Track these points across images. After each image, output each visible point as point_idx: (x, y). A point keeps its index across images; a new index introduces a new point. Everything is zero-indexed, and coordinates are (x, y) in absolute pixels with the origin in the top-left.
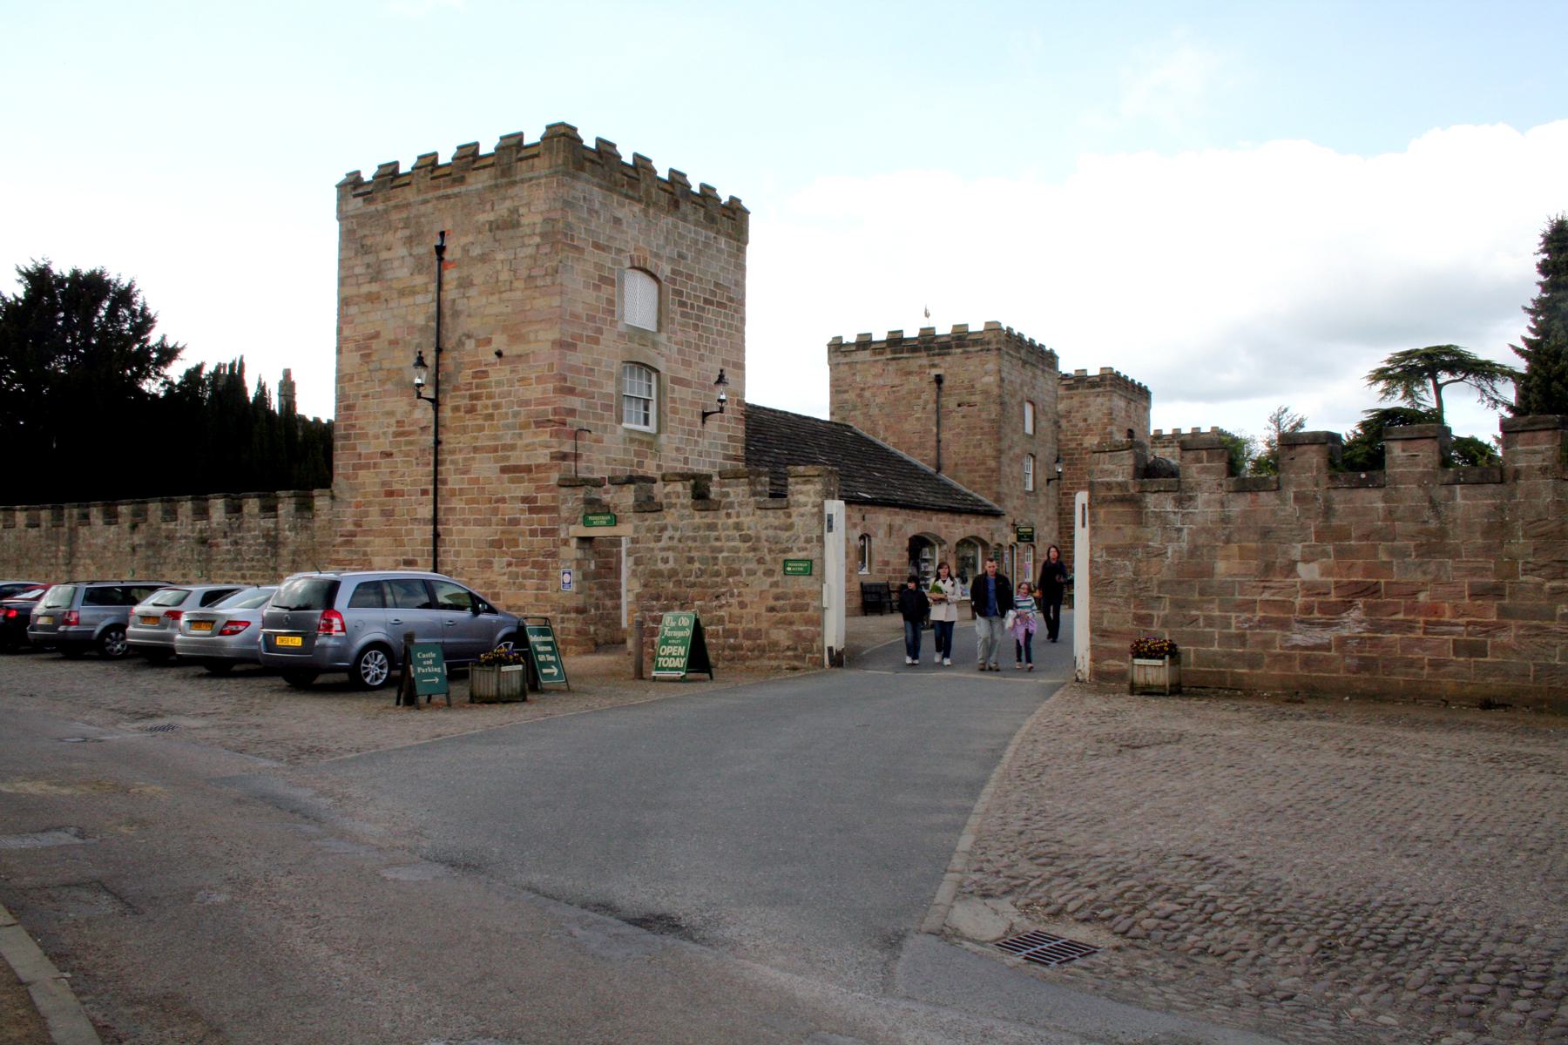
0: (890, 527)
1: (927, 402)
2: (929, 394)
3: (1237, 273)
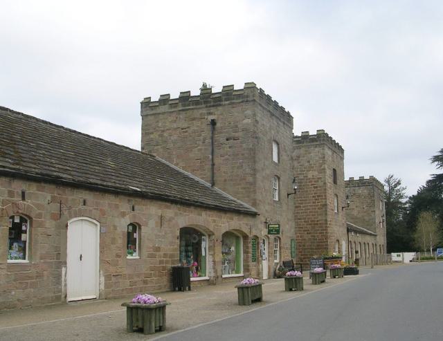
0: (161, 217)
1: (204, 140)
2: (207, 133)
3: (387, 151)
